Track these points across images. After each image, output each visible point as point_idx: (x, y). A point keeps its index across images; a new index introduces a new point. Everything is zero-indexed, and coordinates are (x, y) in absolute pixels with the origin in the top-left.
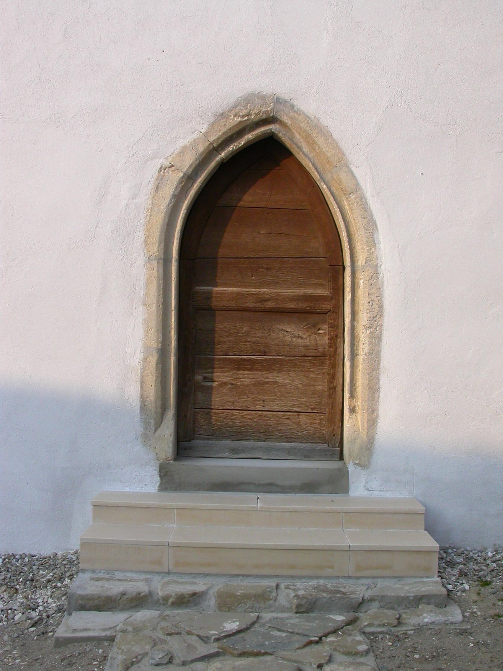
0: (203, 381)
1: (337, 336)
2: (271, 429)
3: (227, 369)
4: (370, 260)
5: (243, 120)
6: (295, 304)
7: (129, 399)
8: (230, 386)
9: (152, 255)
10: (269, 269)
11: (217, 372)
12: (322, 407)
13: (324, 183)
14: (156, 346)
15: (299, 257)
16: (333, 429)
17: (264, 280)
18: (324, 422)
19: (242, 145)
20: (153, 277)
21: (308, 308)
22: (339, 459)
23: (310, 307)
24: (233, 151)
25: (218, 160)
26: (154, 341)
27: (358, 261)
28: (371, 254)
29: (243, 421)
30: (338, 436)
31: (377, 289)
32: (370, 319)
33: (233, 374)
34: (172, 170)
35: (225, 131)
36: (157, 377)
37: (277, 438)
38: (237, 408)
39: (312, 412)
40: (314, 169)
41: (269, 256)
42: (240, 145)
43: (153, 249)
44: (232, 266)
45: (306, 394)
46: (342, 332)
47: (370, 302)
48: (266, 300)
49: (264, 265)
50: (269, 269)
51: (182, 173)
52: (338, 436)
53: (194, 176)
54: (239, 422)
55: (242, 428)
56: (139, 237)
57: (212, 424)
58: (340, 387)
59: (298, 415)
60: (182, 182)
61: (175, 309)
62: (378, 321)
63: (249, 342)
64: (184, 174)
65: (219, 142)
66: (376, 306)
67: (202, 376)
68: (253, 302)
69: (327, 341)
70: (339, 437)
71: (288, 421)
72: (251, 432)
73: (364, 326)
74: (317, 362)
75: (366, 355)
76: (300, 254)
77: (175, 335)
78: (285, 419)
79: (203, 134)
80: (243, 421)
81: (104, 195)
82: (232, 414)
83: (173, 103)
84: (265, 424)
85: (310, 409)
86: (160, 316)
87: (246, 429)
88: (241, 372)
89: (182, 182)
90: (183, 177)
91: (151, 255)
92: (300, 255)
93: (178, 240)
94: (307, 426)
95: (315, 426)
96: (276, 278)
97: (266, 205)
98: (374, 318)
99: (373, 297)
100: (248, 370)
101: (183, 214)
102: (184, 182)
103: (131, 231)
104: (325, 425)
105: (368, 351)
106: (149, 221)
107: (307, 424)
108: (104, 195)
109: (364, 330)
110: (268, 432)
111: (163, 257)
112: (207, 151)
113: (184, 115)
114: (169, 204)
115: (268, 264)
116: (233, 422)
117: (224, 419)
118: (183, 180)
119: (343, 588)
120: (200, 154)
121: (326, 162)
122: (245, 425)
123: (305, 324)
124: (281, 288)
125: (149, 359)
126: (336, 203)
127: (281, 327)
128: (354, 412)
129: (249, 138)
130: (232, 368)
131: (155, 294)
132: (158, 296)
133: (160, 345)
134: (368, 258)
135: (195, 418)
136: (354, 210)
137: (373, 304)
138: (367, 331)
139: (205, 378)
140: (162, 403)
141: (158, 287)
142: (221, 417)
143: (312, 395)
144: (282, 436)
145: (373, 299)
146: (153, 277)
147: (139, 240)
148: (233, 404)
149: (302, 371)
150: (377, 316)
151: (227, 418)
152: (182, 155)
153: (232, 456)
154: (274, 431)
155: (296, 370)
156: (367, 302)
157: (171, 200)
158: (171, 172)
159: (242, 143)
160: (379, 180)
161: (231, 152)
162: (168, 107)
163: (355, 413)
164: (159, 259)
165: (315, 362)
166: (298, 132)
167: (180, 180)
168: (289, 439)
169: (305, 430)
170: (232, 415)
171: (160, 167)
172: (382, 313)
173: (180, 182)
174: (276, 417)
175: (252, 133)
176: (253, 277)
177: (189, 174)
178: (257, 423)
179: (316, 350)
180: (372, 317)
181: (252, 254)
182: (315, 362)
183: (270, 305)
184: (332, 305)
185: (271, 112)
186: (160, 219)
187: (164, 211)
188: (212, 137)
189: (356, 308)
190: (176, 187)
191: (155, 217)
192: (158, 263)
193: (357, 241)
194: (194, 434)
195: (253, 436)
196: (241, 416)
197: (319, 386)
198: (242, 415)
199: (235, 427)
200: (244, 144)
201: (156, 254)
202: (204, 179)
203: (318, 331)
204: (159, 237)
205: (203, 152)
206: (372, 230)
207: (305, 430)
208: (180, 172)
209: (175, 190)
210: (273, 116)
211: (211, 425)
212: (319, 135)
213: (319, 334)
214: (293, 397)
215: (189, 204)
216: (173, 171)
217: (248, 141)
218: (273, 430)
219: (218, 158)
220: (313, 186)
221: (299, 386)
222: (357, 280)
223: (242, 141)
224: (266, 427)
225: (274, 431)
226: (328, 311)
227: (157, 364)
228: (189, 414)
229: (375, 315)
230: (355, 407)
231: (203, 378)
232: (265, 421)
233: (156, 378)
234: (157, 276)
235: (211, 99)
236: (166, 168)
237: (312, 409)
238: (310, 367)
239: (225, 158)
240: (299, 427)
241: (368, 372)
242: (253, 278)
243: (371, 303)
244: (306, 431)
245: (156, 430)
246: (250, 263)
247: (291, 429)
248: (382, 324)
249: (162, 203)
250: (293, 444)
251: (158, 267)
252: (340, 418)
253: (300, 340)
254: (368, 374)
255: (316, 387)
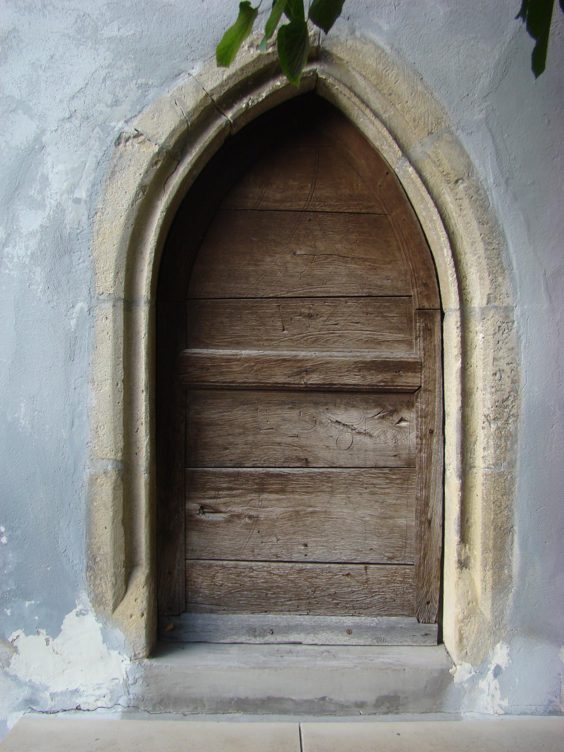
0: (200, 513)
1: (432, 432)
2: (318, 592)
3: (241, 491)
4: (495, 298)
5: (266, 52)
6: (359, 377)
7: (67, 551)
8: (247, 520)
9: (103, 293)
10: (312, 316)
11: (224, 497)
12: (406, 554)
13: (410, 162)
14: (112, 457)
15: (364, 295)
16: (427, 592)
17: (304, 337)
18: (410, 580)
19: (263, 100)
20: (105, 332)
21: (382, 384)
22: (436, 644)
23: (385, 382)
24: (248, 109)
25: (222, 125)
26: (109, 448)
27: (472, 300)
28: (496, 288)
29: (270, 580)
30: (434, 604)
31: (509, 350)
32: (497, 404)
33: (252, 500)
34: (140, 140)
35: (234, 72)
36: (115, 512)
37: (329, 608)
38: (259, 558)
39: (389, 562)
40: (391, 138)
41: (311, 295)
42: (260, 99)
43: (106, 282)
44: (247, 311)
45: (379, 532)
46: (441, 424)
47: (496, 374)
48: (307, 372)
49: (303, 310)
50: (312, 316)
51: (157, 146)
52: (434, 604)
53: (179, 153)
54: (263, 582)
55: (268, 592)
56: (81, 261)
57: (217, 585)
58: (437, 521)
59: (366, 568)
60: (156, 163)
61: (147, 388)
62: (510, 407)
63: (279, 444)
64: (161, 149)
65: (223, 92)
66: (507, 381)
67: (197, 503)
68: (285, 375)
69: (415, 440)
70: (437, 606)
71: (348, 579)
72: (284, 598)
73: (486, 416)
74: (398, 476)
75: (490, 468)
76: (365, 291)
77: (147, 436)
78: (343, 575)
79: (194, 77)
80: (270, 580)
81: (18, 187)
82: (251, 568)
83: (141, 24)
84: (308, 584)
85: (386, 558)
86: (119, 403)
87: (274, 593)
88: (265, 496)
89: (156, 163)
90: (158, 154)
91: (101, 292)
92: (365, 292)
93: (151, 266)
94: (381, 586)
95: (394, 586)
96: (324, 332)
97: (305, 208)
98: (503, 401)
99: (502, 364)
100: (277, 492)
101: (159, 219)
102: (161, 162)
103: (66, 249)
104: (411, 585)
105: (494, 461)
106: (98, 232)
107: (380, 584)
108: (18, 187)
109: (487, 423)
110: (314, 598)
111: (123, 297)
112: (202, 108)
113: (159, 45)
114: (134, 201)
115: (310, 308)
116: (253, 581)
117: (238, 576)
118: (159, 159)
119: (346, 634)
120: (189, 112)
121: (412, 127)
122: (273, 587)
123: (376, 411)
124: (334, 350)
125: (99, 480)
126: (432, 198)
127: (334, 418)
128: (466, 568)
129: (276, 86)
130: (248, 489)
131: (110, 363)
132: (115, 366)
133: (120, 455)
134: (491, 296)
135: (187, 575)
136: (464, 210)
137: (501, 377)
138: (492, 425)
139: (203, 507)
140: (126, 556)
141: (115, 350)
142: (231, 574)
143: (390, 533)
144: (338, 604)
145: (501, 368)
146: (105, 332)
147: (81, 266)
148: (253, 551)
149: (373, 493)
150: (508, 397)
151: (243, 574)
152: (156, 115)
153: (253, 640)
154: (324, 596)
155: (362, 491)
156: (491, 374)
157: (137, 194)
158: (137, 146)
159: (264, 95)
160: (508, 157)
161: (243, 110)
162: (132, 32)
163: (469, 569)
164: (116, 300)
165: (394, 477)
166: (361, 75)
167: (153, 159)
168: (350, 609)
169: (378, 593)
170: (251, 570)
171: (118, 136)
172: (517, 392)
173: (153, 163)
174: (327, 573)
175: (280, 78)
176: (284, 330)
177: (170, 148)
178: (294, 583)
179: (395, 456)
180: (500, 400)
181: (283, 291)
182: (394, 477)
183: (314, 379)
184: (423, 377)
185: (315, 40)
186: (118, 228)
187: (124, 214)
188: (210, 83)
189: (470, 385)
190: (147, 172)
191: (108, 225)
192: (114, 306)
193: (469, 265)
194: (186, 559)
195: (287, 605)
196: (267, 571)
197: (400, 517)
198: (269, 569)
199: (257, 589)
200: (267, 97)
201: (111, 291)
202: (196, 158)
203: (398, 423)
204: (116, 261)
205: (195, 109)
206: (498, 244)
207: (378, 593)
208: (154, 144)
209: (145, 177)
210: (319, 46)
211: (216, 587)
212: (401, 79)
213: (400, 427)
214: (356, 538)
215: (169, 201)
216: (141, 142)
217: (273, 91)
218: (323, 594)
219: (221, 122)
220: (387, 174)
221: (367, 519)
222: (472, 335)
223: (263, 92)
224: (310, 591)
225: (324, 596)
226: (416, 388)
227: (114, 489)
228: (176, 571)
229: (505, 397)
230: (468, 558)
231: (199, 507)
232: (309, 580)
233: (114, 515)
234: (111, 330)
235: (208, 17)
236: (129, 138)
237: (390, 558)
238: (385, 486)
239: (234, 121)
240: (366, 589)
241: (494, 498)
242: (285, 332)
243: (497, 375)
244: (379, 595)
245: (115, 607)
246: (279, 306)
247: (353, 592)
248: (517, 412)
249: (122, 200)
250: (357, 619)
251: (114, 314)
252: (438, 574)
253: (367, 440)
254: (494, 503)
255: (396, 519)
